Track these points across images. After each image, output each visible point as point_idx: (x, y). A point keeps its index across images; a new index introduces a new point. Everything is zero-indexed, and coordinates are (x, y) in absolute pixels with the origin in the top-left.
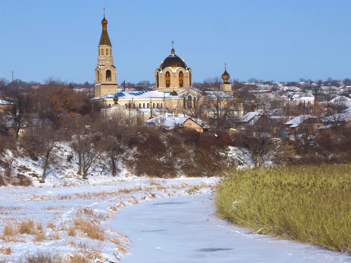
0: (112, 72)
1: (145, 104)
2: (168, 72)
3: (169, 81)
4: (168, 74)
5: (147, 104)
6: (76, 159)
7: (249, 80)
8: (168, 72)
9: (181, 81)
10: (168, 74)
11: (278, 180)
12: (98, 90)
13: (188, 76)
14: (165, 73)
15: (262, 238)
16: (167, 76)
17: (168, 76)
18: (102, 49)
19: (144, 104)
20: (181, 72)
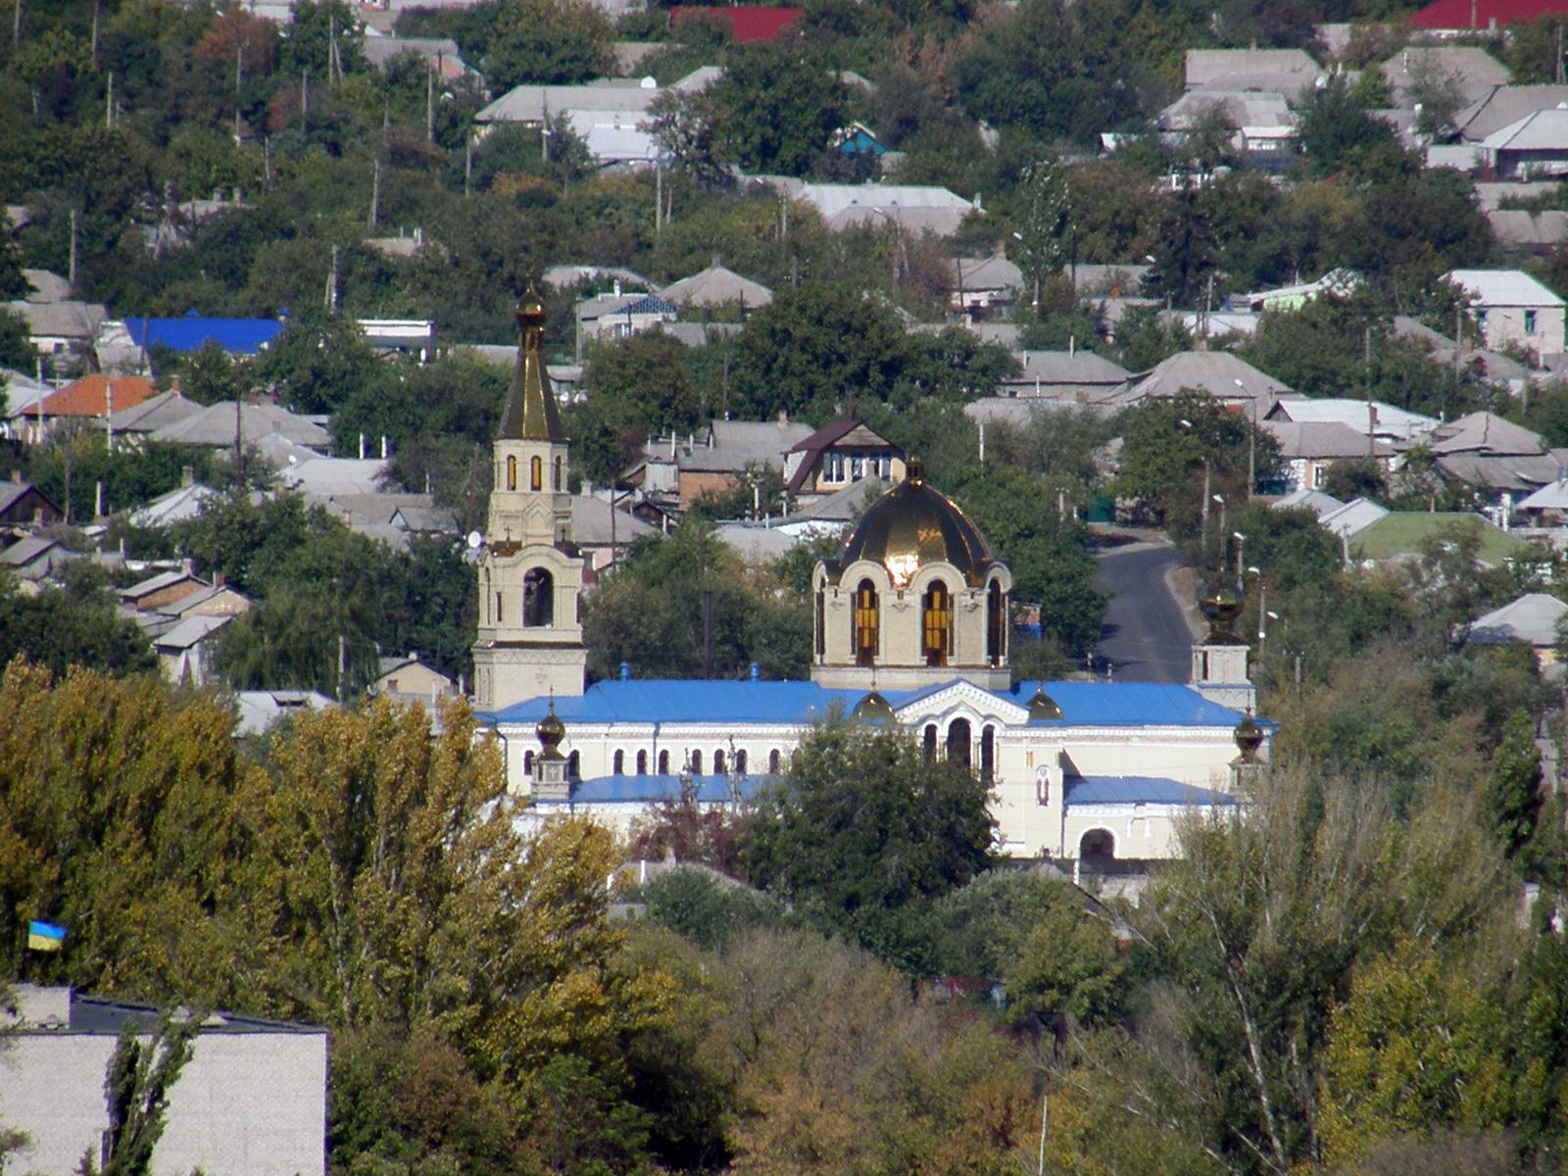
0: (556, 582)
1: (704, 755)
2: (867, 584)
3: (874, 634)
4: (867, 594)
5: (712, 755)
6: (368, 1019)
7: (163, 1118)
8: (867, 584)
9: (937, 634)
10: (867, 594)
11: (1351, 866)
12: (484, 668)
13: (976, 606)
14: (855, 589)
15: (1309, 838)
16: (861, 605)
17: (867, 604)
18: (511, 457)
19: (642, 756)
20: (937, 585)
